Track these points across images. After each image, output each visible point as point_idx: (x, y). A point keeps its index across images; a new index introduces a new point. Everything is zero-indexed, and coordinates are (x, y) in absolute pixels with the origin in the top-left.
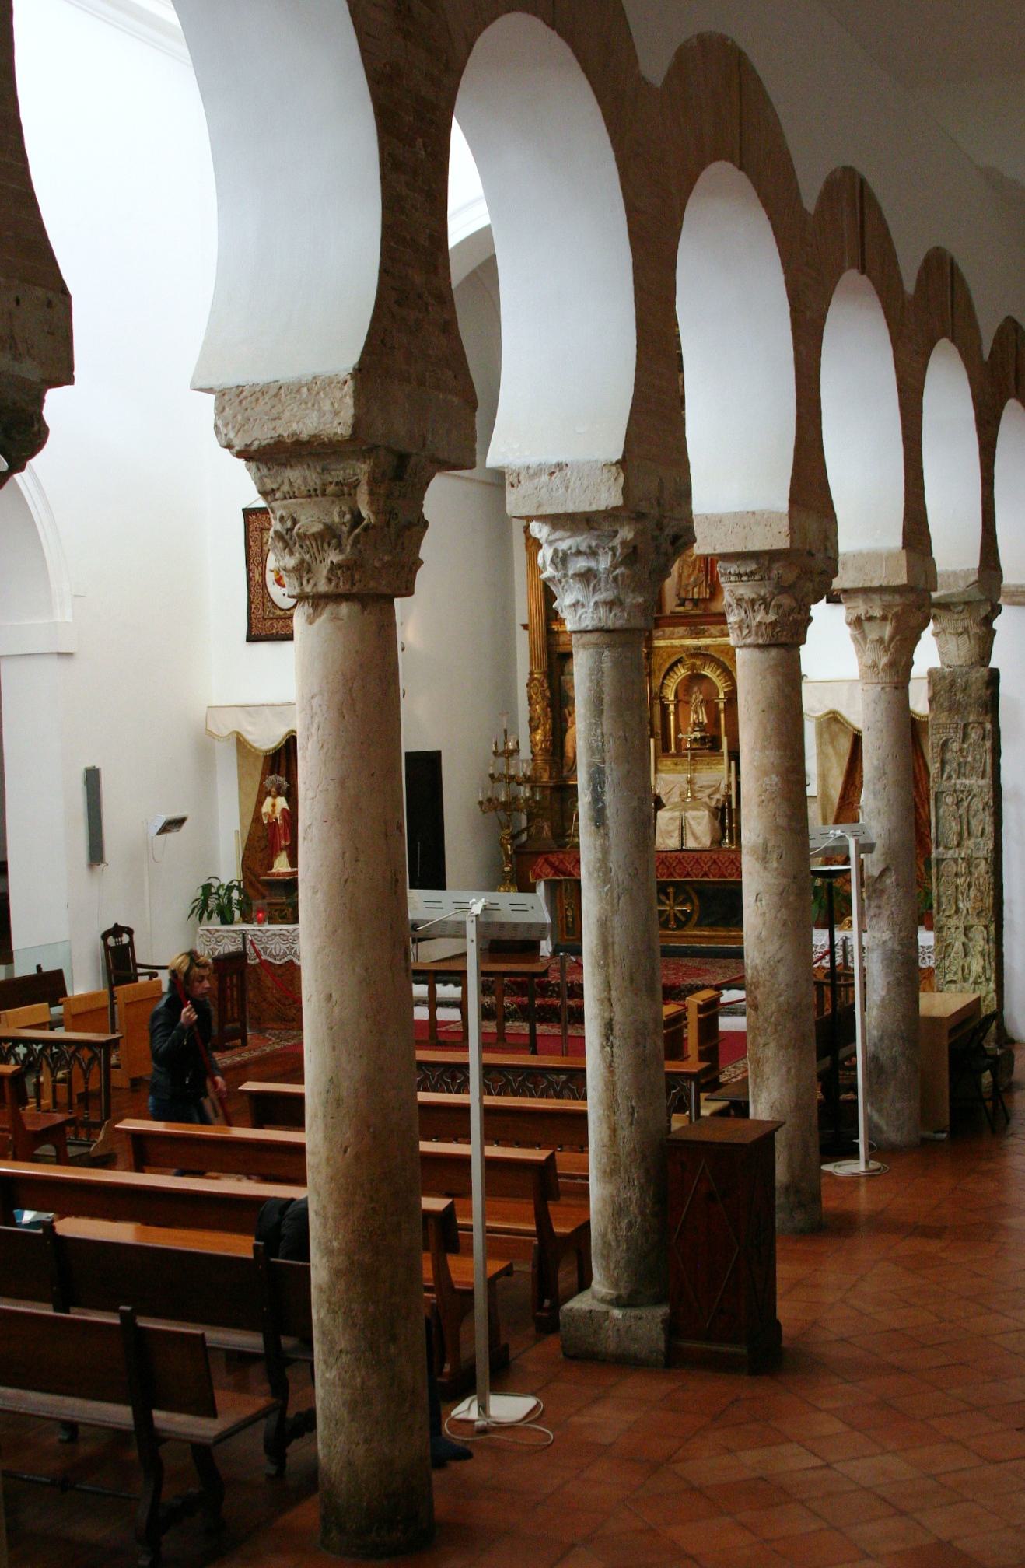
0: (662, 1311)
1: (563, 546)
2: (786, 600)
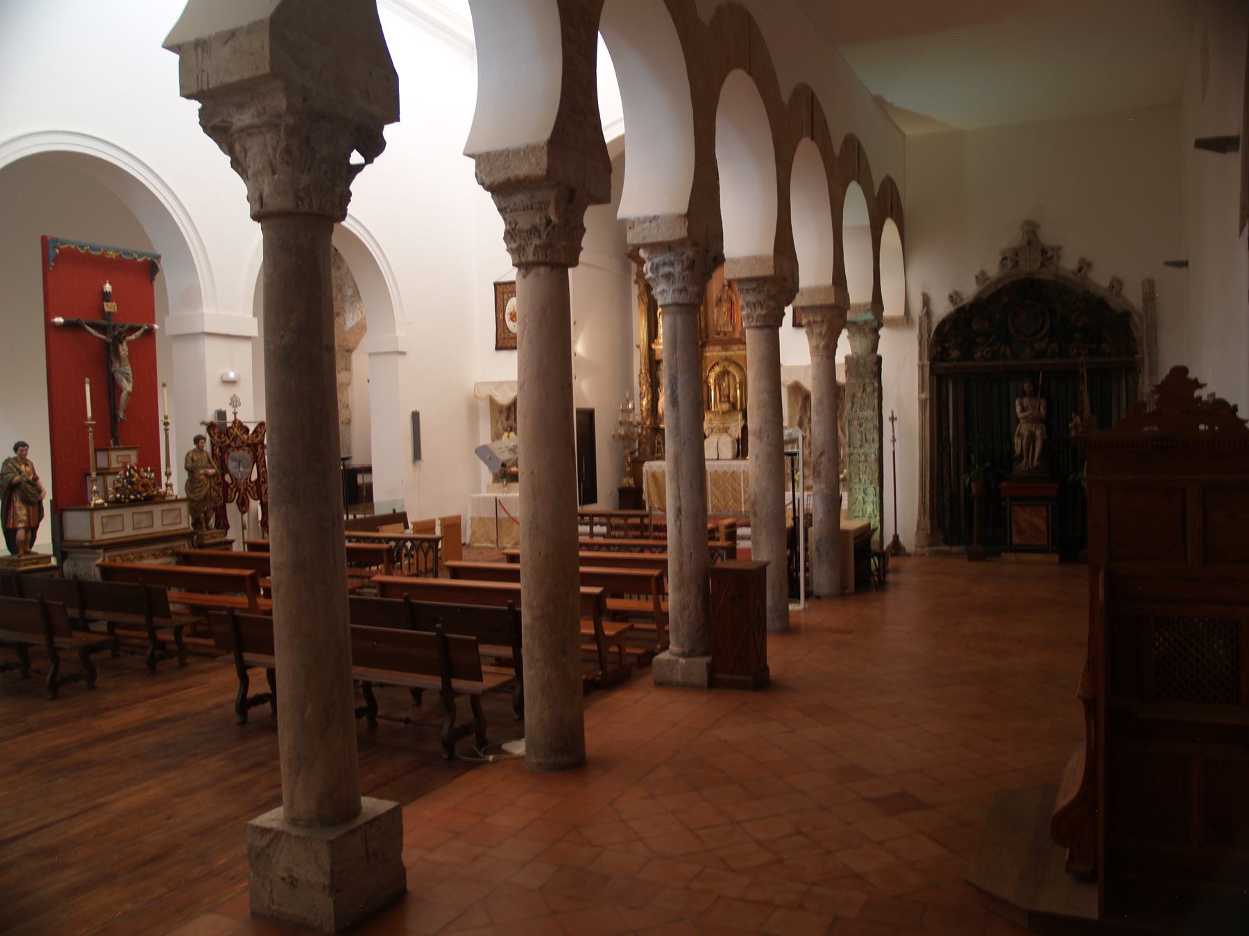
0: (708, 659)
1: (656, 260)
2: (772, 303)
